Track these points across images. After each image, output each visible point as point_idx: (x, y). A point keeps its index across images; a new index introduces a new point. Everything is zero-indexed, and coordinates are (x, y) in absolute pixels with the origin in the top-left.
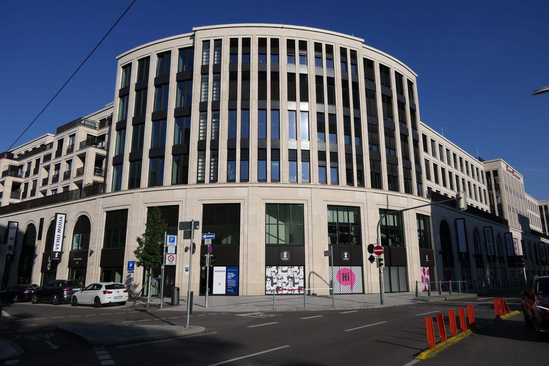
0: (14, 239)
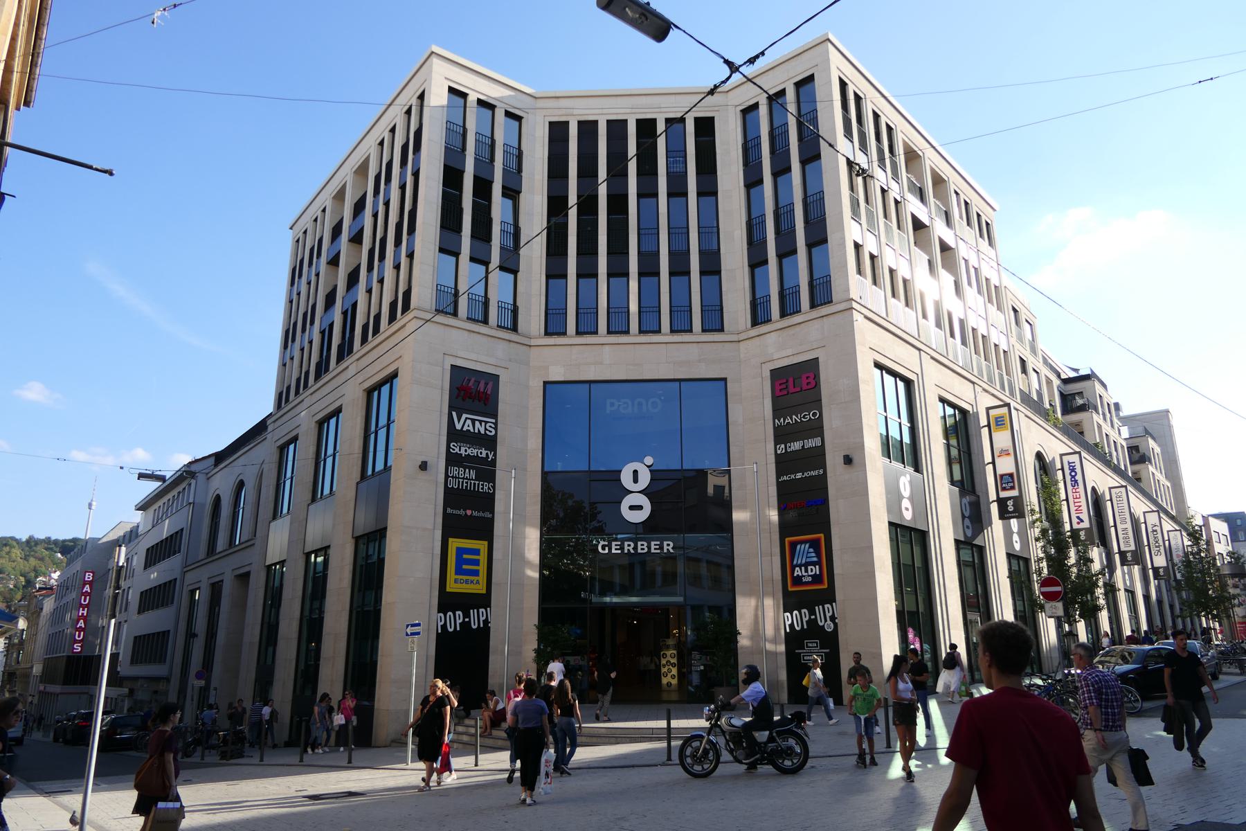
0: (1011, 451)
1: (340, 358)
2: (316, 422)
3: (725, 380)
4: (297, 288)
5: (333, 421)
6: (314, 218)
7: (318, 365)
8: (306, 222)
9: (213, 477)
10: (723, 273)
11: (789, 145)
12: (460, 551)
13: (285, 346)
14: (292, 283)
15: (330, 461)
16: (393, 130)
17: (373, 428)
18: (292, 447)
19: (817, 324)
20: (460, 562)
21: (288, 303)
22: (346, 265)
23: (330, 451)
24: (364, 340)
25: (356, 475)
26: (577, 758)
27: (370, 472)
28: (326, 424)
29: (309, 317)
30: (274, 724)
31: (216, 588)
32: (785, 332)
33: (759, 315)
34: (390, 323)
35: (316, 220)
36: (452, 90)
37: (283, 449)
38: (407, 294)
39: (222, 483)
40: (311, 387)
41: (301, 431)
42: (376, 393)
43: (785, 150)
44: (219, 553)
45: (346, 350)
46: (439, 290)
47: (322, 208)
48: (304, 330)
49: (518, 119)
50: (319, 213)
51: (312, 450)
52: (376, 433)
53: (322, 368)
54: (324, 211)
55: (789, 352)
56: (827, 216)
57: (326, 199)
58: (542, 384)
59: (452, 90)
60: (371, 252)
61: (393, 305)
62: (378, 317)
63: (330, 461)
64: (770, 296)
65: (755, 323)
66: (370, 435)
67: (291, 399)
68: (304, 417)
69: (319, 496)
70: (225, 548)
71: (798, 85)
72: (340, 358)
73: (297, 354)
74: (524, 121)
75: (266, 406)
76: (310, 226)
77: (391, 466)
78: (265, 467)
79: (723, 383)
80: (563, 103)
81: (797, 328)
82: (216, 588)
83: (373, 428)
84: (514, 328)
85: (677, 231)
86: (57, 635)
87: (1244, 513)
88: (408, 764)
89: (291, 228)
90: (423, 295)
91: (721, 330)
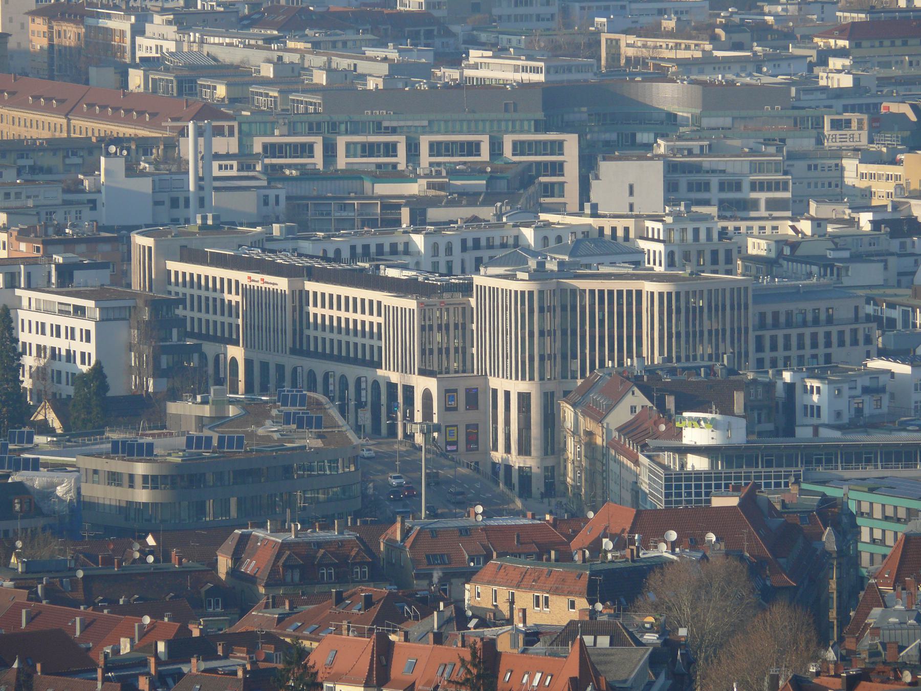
12: (450, 431)
20: (450, 433)
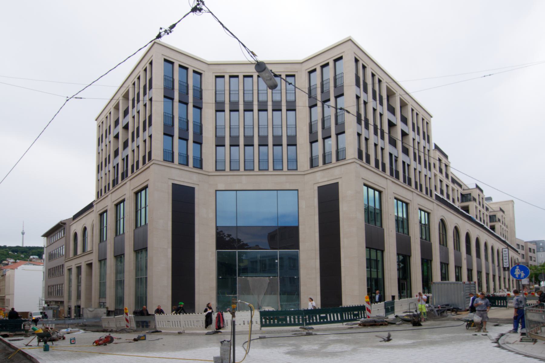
1: (123, 179)
2: (134, 193)
3: (297, 190)
4: (101, 148)
5: (122, 204)
6: (106, 116)
7: (114, 181)
8: (103, 117)
9: (73, 225)
10: (298, 145)
11: (343, 83)
13: (98, 172)
14: (99, 145)
15: (143, 210)
16: (139, 78)
17: (139, 208)
18: (105, 214)
19: (338, 168)
21: (98, 154)
22: (122, 138)
23: (143, 205)
24: (133, 171)
25: (133, 227)
26: (136, 335)
27: (139, 226)
28: (119, 206)
29: (108, 160)
30: (214, 304)
31: (79, 268)
32: (325, 172)
33: (313, 164)
34: (132, 173)
35: (107, 117)
36: (166, 60)
37: (101, 215)
38: (150, 153)
39: (77, 227)
40: (111, 190)
41: (108, 208)
42: (139, 194)
43: (328, 91)
44: (79, 255)
45: (125, 175)
46: (165, 152)
47: (109, 112)
48: (106, 166)
49: (200, 74)
50: (108, 114)
51: (114, 216)
52: (141, 210)
53: (115, 182)
54: (110, 113)
55: (326, 179)
56: (345, 121)
57: (111, 108)
58: (215, 191)
59: (166, 60)
60: (133, 133)
61: (144, 157)
62: (138, 162)
63: (143, 210)
64: (331, 152)
65: (312, 166)
66: (138, 211)
67: (110, 189)
68: (109, 202)
69: (119, 234)
70: (81, 253)
71: (336, 61)
72: (123, 179)
73: (103, 176)
74: (203, 76)
75: (91, 197)
76: (104, 120)
77: (147, 224)
78: (94, 222)
79: (296, 191)
80: (222, 67)
81: (330, 170)
82: (79, 268)
83: (139, 208)
84: (201, 168)
85: (277, 126)
86: (57, 268)
87: (544, 241)
88: (304, 326)
89: (96, 120)
90: (158, 154)
91: (297, 169)
